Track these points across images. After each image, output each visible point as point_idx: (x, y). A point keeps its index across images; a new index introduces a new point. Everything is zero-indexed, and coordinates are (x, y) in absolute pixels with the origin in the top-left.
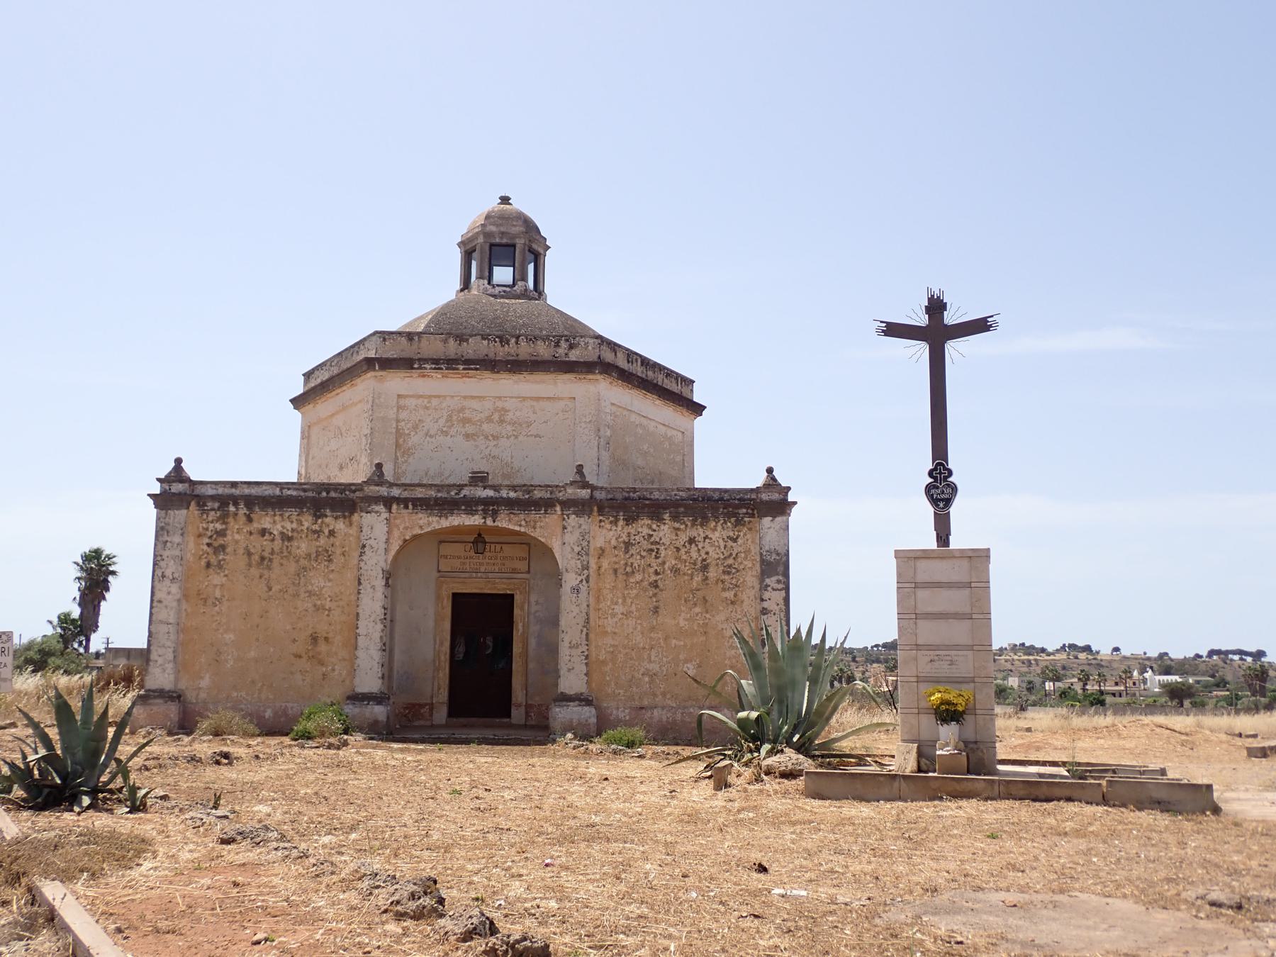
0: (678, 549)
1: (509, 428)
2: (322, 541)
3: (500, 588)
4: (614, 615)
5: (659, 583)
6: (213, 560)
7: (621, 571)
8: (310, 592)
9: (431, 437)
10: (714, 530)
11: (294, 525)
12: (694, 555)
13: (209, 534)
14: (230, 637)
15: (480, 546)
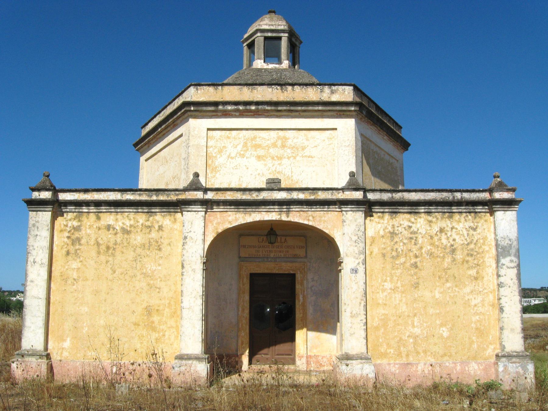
0: (432, 237)
1: (289, 151)
2: (154, 235)
3: (285, 268)
4: (384, 290)
5: (419, 264)
6: (72, 249)
7: (389, 255)
8: (145, 274)
9: (232, 158)
10: (459, 221)
11: (132, 222)
12: (444, 241)
13: (68, 229)
14: (85, 309)
15: (273, 238)
